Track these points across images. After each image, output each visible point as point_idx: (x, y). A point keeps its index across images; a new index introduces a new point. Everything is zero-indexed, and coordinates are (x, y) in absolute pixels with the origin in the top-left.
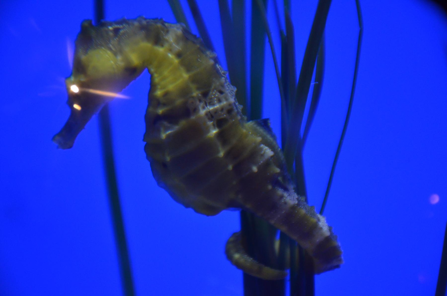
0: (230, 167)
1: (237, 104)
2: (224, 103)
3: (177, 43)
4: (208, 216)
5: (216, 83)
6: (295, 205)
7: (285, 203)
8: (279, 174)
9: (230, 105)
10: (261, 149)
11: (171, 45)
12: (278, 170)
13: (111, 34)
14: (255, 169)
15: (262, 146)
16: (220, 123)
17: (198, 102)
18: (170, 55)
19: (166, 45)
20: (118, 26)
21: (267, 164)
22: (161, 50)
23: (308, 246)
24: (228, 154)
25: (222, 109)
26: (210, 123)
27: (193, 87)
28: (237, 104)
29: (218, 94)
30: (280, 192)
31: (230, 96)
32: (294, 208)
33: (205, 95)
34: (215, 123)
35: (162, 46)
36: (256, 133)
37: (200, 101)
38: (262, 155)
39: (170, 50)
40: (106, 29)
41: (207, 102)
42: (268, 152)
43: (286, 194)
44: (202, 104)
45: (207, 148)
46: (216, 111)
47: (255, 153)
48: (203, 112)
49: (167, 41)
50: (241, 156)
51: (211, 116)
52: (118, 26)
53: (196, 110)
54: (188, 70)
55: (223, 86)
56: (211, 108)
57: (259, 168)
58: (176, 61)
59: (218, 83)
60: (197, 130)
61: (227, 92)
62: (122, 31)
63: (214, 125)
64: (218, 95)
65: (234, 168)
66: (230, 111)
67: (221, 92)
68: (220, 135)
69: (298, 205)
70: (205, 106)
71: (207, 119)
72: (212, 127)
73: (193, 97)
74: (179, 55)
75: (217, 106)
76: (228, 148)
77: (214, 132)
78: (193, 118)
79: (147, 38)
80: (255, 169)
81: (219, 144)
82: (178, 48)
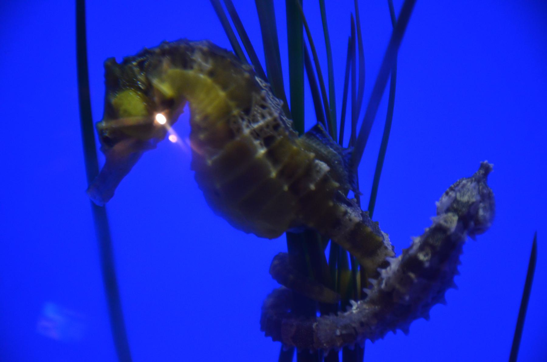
0: (286, 188)
1: (284, 118)
2: (269, 118)
3: (206, 61)
4: (270, 239)
5: (256, 97)
6: (360, 221)
7: (350, 220)
8: (340, 188)
9: (275, 120)
10: (317, 165)
11: (200, 65)
12: (337, 184)
13: (136, 70)
14: (312, 187)
15: (317, 161)
16: (268, 141)
17: (240, 120)
18: (202, 76)
19: (196, 66)
20: (142, 59)
21: (325, 179)
22: (191, 73)
23: (449, 233)
24: (281, 174)
25: (267, 126)
26: (257, 143)
27: (232, 104)
28: (284, 118)
29: (261, 109)
30: (343, 207)
31: (274, 108)
32: (359, 225)
33: (247, 111)
34: (262, 142)
35: (192, 68)
36: (309, 148)
37: (243, 119)
38: (318, 172)
39: (201, 71)
40: (130, 65)
41: (251, 119)
42: (324, 167)
43: (349, 210)
44: (245, 123)
45: (257, 171)
46: (261, 129)
47: (310, 170)
48: (247, 131)
49: (194, 61)
50: (297, 175)
51: (256, 134)
52: (142, 59)
53: (239, 130)
54: (224, 87)
55: (264, 99)
56: (256, 126)
57: (316, 186)
58: (209, 80)
59: (258, 98)
60: (244, 152)
61: (269, 106)
62: (146, 64)
63: (261, 144)
64: (260, 110)
65: (290, 188)
66: (276, 127)
67: (263, 107)
68: (270, 154)
69: (364, 221)
70: (248, 124)
71: (252, 139)
72: (259, 146)
73: (234, 116)
74: (211, 74)
75: (261, 123)
76: (280, 167)
77: (262, 151)
78: (238, 139)
79: (174, 63)
80: (312, 187)
81: (269, 164)
82: (208, 66)
